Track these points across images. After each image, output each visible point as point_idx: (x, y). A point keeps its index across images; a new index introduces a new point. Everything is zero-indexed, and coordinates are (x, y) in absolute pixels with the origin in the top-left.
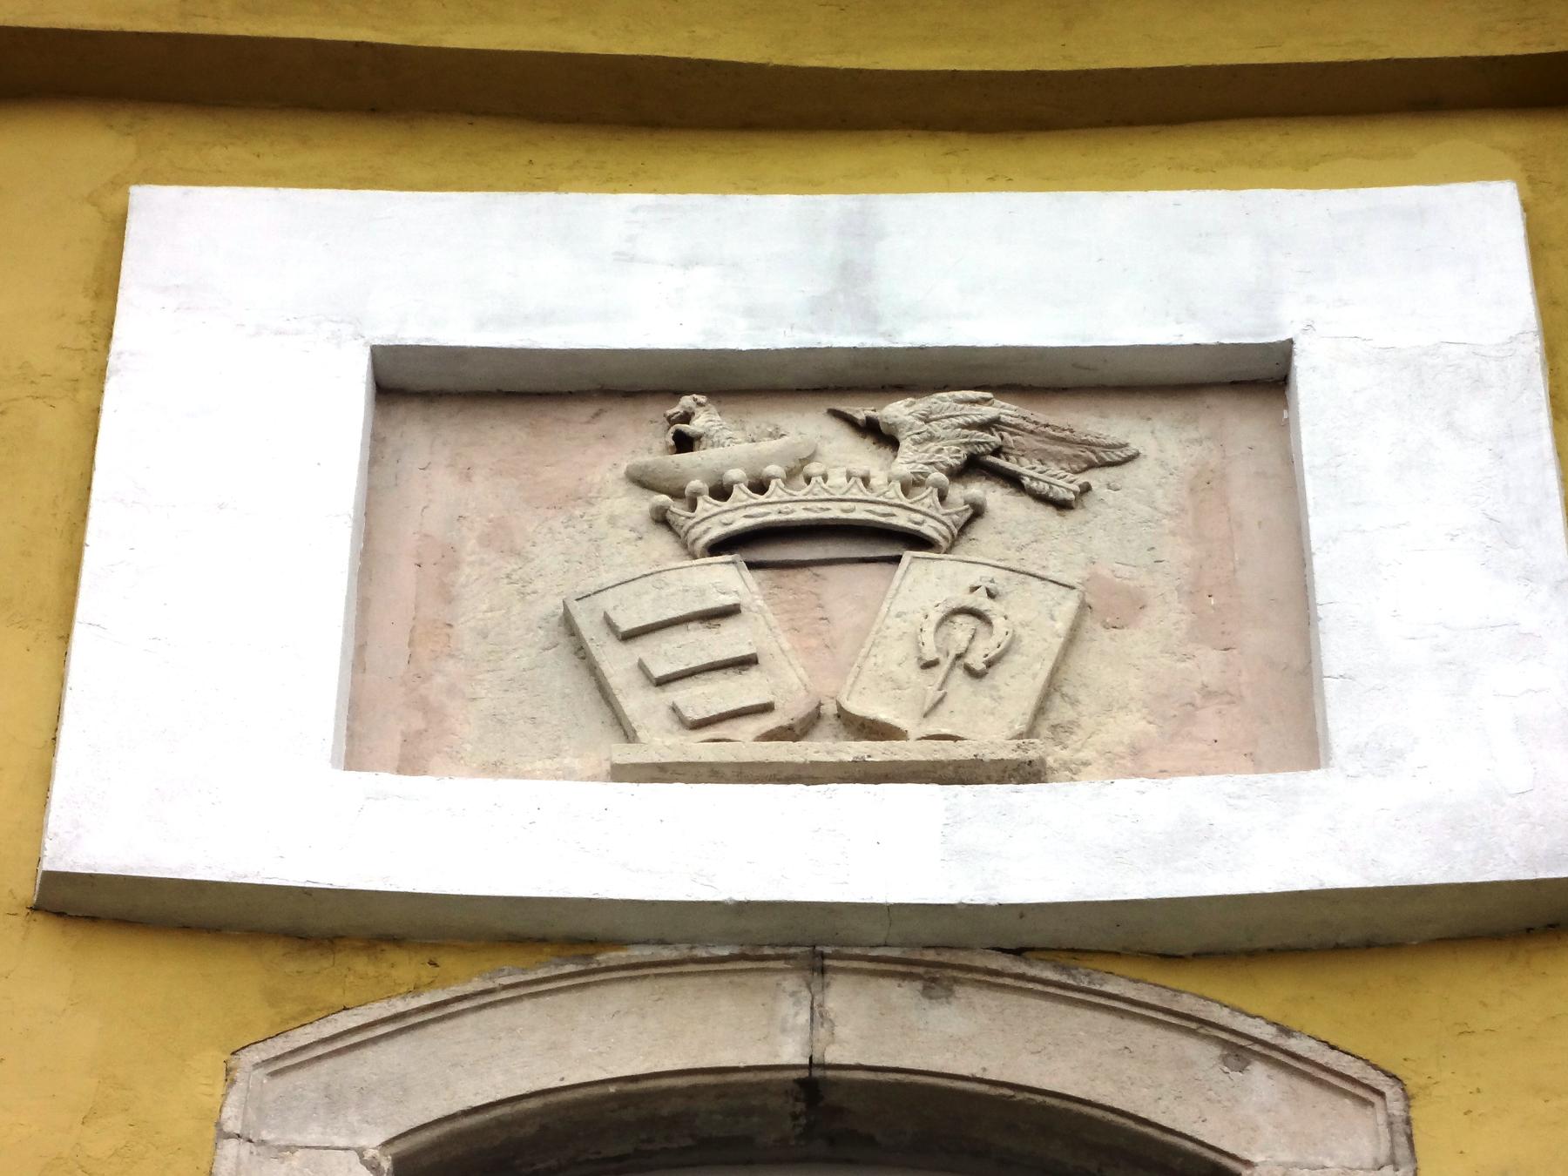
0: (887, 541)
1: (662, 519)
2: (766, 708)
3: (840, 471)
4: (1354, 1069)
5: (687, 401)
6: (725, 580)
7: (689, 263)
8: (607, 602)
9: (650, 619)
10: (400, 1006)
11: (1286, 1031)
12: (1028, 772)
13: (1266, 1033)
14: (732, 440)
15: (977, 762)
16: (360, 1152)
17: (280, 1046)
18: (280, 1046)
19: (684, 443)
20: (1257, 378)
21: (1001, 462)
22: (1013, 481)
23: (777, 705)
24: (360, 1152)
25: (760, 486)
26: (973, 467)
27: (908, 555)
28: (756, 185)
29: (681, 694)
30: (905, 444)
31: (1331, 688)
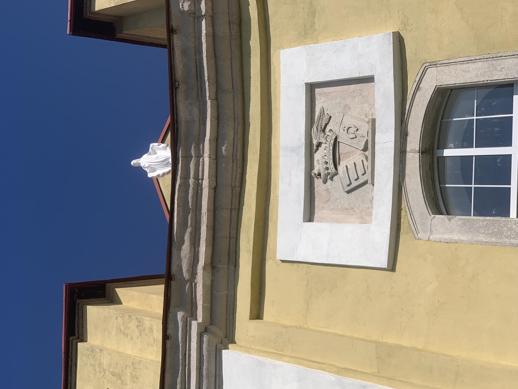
0: (336, 143)
1: (332, 179)
2: (362, 161)
3: (322, 156)
5: (312, 174)
6: (341, 168)
8: (345, 186)
10: (409, 214)
11: (415, 81)
12: (374, 121)
13: (415, 84)
14: (318, 167)
15: (372, 128)
16: (432, 219)
17: (415, 232)
18: (415, 232)
19: (319, 174)
20: (311, 88)
21: (323, 127)
22: (326, 125)
23: (256, 323)
24: (432, 219)
26: (324, 131)
27: (338, 140)
28: (277, 166)
29: (360, 175)
31: (361, 75)
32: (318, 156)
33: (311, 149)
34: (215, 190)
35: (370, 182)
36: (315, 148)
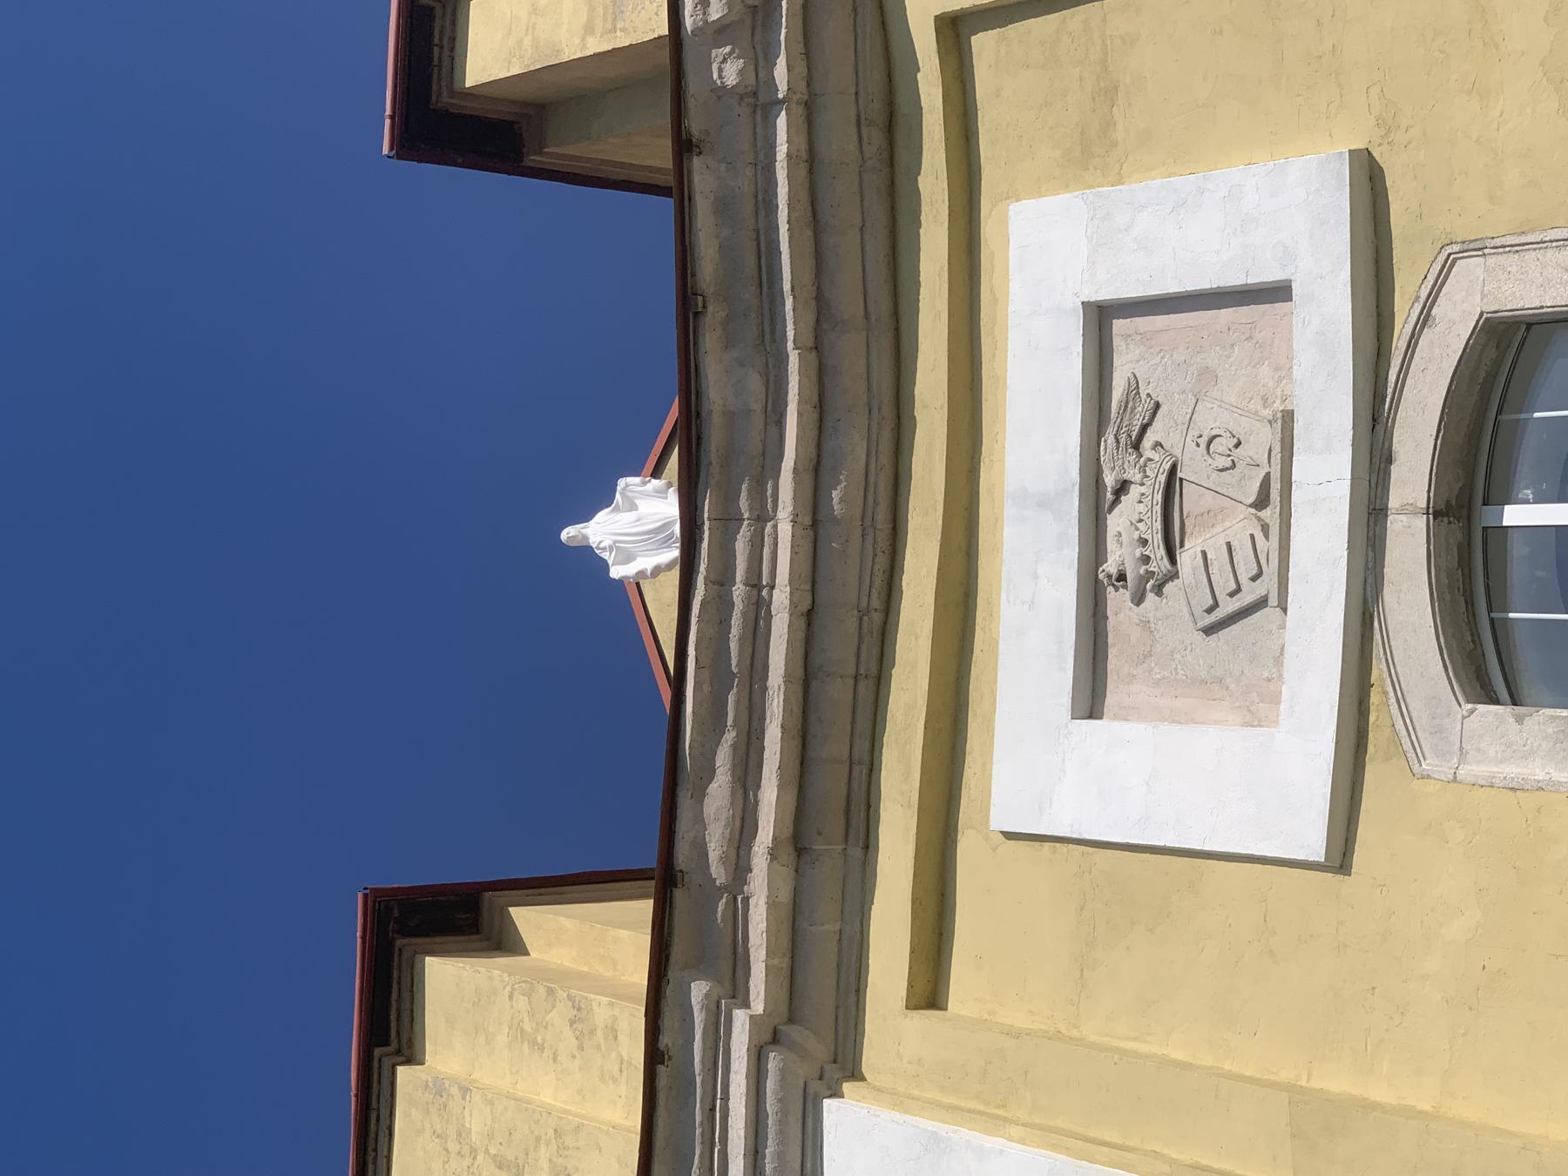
1: (1159, 590)
2: (1252, 537)
3: (1131, 521)
4: (1437, 267)
5: (1101, 576)
6: (1188, 559)
7: (1035, 576)
8: (1198, 611)
9: (1208, 590)
10: (1393, 700)
12: (1288, 418)
13: (1418, 308)
15: (1282, 441)
16: (1464, 718)
17: (1411, 754)
19: (1122, 577)
20: (1101, 319)
22: (1144, 429)
25: (1144, 542)
27: (1179, 475)
28: (997, 549)
29: (1244, 579)
30: (1125, 476)
32: (1117, 522)
33: (1097, 501)
34: (809, 618)
35: (1273, 600)
36: (1109, 496)
